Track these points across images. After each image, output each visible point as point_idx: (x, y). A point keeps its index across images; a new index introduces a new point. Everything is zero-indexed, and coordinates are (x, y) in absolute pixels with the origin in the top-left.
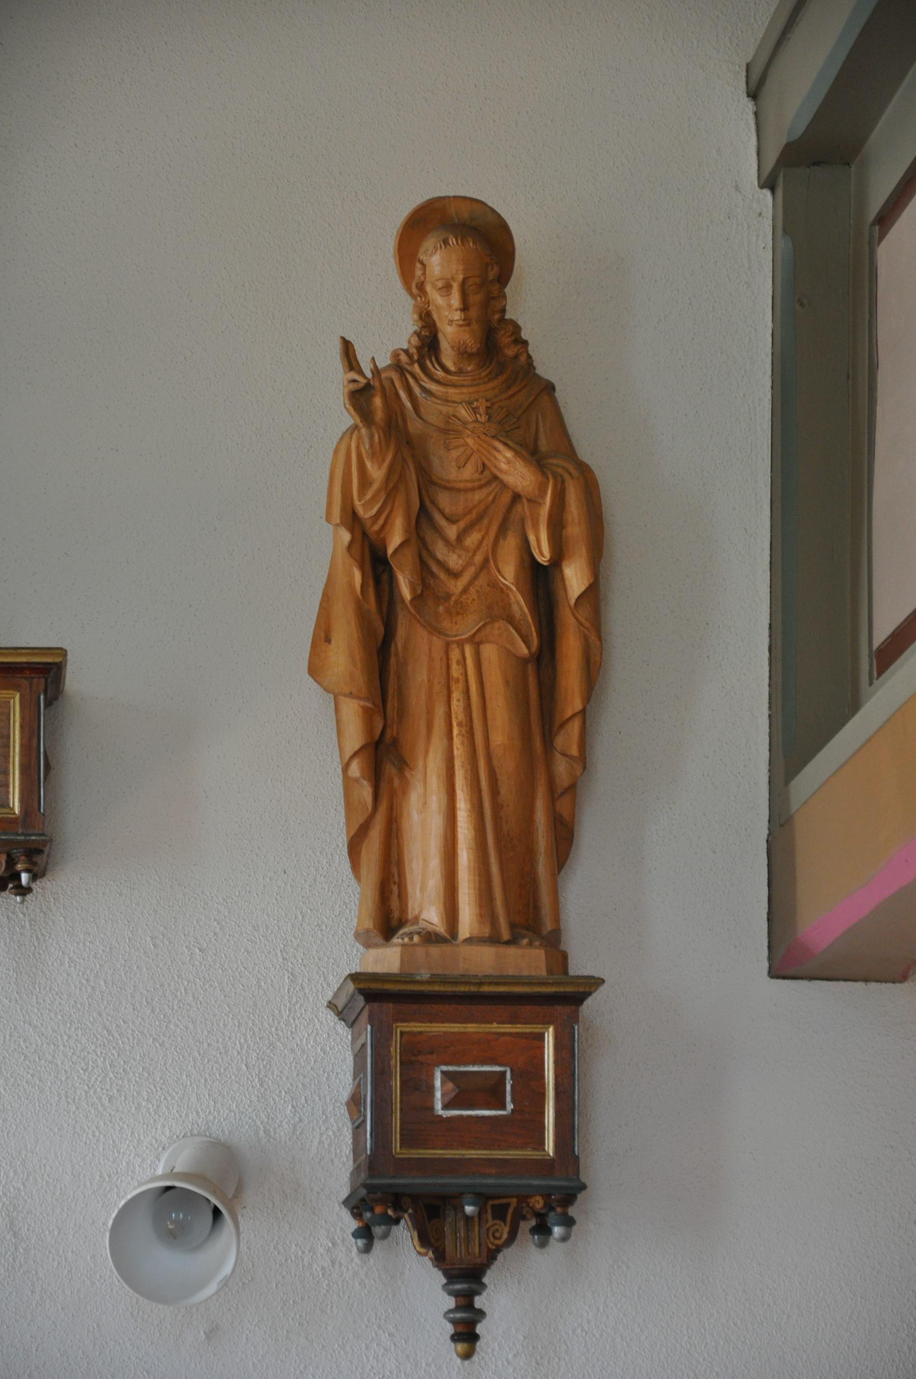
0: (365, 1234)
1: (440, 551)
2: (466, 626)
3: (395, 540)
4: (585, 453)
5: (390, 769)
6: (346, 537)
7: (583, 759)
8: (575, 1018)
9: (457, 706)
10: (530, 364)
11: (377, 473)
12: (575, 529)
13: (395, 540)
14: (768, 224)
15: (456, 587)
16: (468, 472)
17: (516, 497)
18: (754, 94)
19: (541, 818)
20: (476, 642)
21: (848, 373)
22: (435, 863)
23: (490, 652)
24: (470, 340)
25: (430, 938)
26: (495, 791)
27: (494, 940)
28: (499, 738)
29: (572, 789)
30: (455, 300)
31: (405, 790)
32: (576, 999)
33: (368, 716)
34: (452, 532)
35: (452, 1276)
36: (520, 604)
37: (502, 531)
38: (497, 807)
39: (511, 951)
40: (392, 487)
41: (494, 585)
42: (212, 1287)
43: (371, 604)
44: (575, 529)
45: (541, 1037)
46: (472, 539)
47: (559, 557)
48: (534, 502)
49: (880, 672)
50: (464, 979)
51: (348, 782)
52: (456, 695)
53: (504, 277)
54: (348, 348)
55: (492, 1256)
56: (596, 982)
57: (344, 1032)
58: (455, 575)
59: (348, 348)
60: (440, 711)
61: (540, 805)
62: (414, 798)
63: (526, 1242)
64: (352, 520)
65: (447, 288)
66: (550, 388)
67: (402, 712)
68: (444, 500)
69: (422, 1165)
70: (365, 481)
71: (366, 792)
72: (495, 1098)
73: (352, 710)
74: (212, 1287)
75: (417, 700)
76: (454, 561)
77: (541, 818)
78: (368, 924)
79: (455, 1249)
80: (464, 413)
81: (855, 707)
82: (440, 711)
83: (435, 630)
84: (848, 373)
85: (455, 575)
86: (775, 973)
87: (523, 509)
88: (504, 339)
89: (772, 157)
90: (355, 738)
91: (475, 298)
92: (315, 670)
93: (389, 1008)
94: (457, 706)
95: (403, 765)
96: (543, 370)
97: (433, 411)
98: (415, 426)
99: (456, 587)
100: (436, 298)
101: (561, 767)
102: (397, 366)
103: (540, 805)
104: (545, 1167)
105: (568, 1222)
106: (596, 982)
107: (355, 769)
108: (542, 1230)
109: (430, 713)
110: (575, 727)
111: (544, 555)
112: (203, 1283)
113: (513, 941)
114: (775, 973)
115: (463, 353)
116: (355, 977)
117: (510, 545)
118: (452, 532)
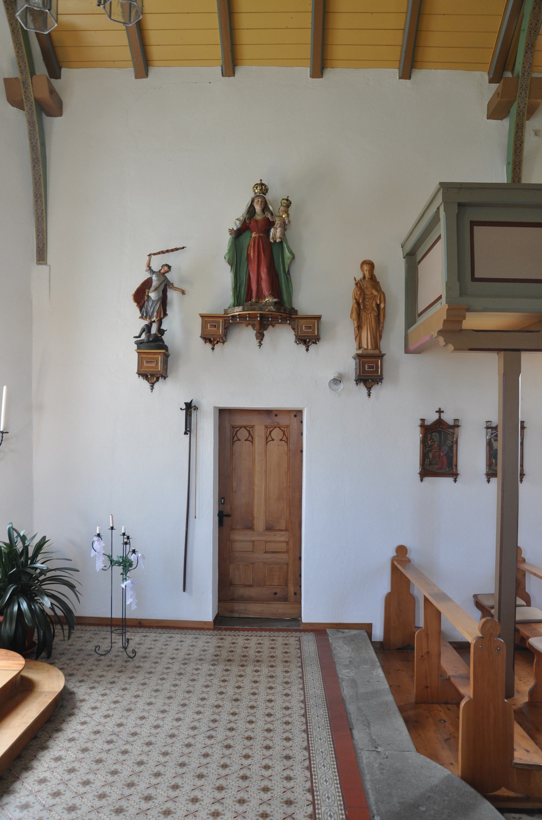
0: (357, 384)
1: (366, 302)
2: (369, 312)
3: (361, 301)
4: (383, 290)
5: (360, 329)
6: (355, 301)
7: (383, 328)
8: (382, 359)
9: (368, 321)
10: (376, 280)
11: (358, 293)
12: (382, 300)
13: (361, 301)
14: (404, 263)
15: (368, 307)
16: (369, 293)
17: (375, 296)
18: (402, 247)
19: (378, 335)
20: (370, 313)
21: (428, 639)
22: (366, 340)
23: (372, 315)
24: (370, 277)
25: (365, 349)
26: (373, 331)
27: (373, 349)
28: (373, 325)
29: (382, 331)
30: (368, 272)
31: (362, 331)
32: (383, 356)
33: (358, 323)
34: (367, 300)
35: (368, 389)
36: (376, 309)
37: (373, 300)
38: (373, 334)
39: (375, 351)
40: (361, 293)
41: (372, 306)
42: (340, 390)
43: (358, 309)
44: (382, 300)
45: (378, 361)
46: (370, 301)
47: (380, 303)
48: (377, 296)
49: (419, 317)
50: (370, 354)
51: (355, 331)
52: (368, 320)
53: (373, 269)
54: (355, 278)
55: (372, 386)
56: (385, 354)
57: (354, 360)
58: (368, 305)
59: (355, 278)
60: (366, 323)
61: (378, 333)
62: (363, 332)
63: (376, 385)
64: (355, 299)
65: (367, 271)
66: (379, 283)
67: (361, 322)
68: (366, 296)
69: (364, 376)
70: (357, 294)
71: (357, 332)
72: (373, 367)
73: (355, 322)
74: (340, 390)
75: (363, 321)
76: (368, 304)
77: (378, 335)
78: (358, 348)
79: (368, 386)
80: (369, 286)
81: (415, 323)
82: (366, 323)
83: (365, 312)
84: (428, 639)
85: (368, 305)
86: (405, 353)
87: (376, 297)
88: (373, 277)
89: (405, 255)
90: (356, 325)
91: (370, 272)
92: (351, 317)
93: (360, 358)
94: (368, 321)
95: (362, 328)
96: (378, 280)
97: (365, 286)
98: (363, 287)
99: (368, 307)
100: (365, 272)
101: (380, 329)
102: (360, 280)
103: (378, 333)
104: (379, 376)
105: (382, 382)
106: (385, 354)
107: (356, 329)
108: (378, 383)
109: (365, 322)
110: (382, 324)
111: (378, 303)
112: (339, 389)
113: (375, 349)
114: (405, 353)
115: (369, 279)
116: (356, 354)
117: (374, 302)
118: (367, 300)
